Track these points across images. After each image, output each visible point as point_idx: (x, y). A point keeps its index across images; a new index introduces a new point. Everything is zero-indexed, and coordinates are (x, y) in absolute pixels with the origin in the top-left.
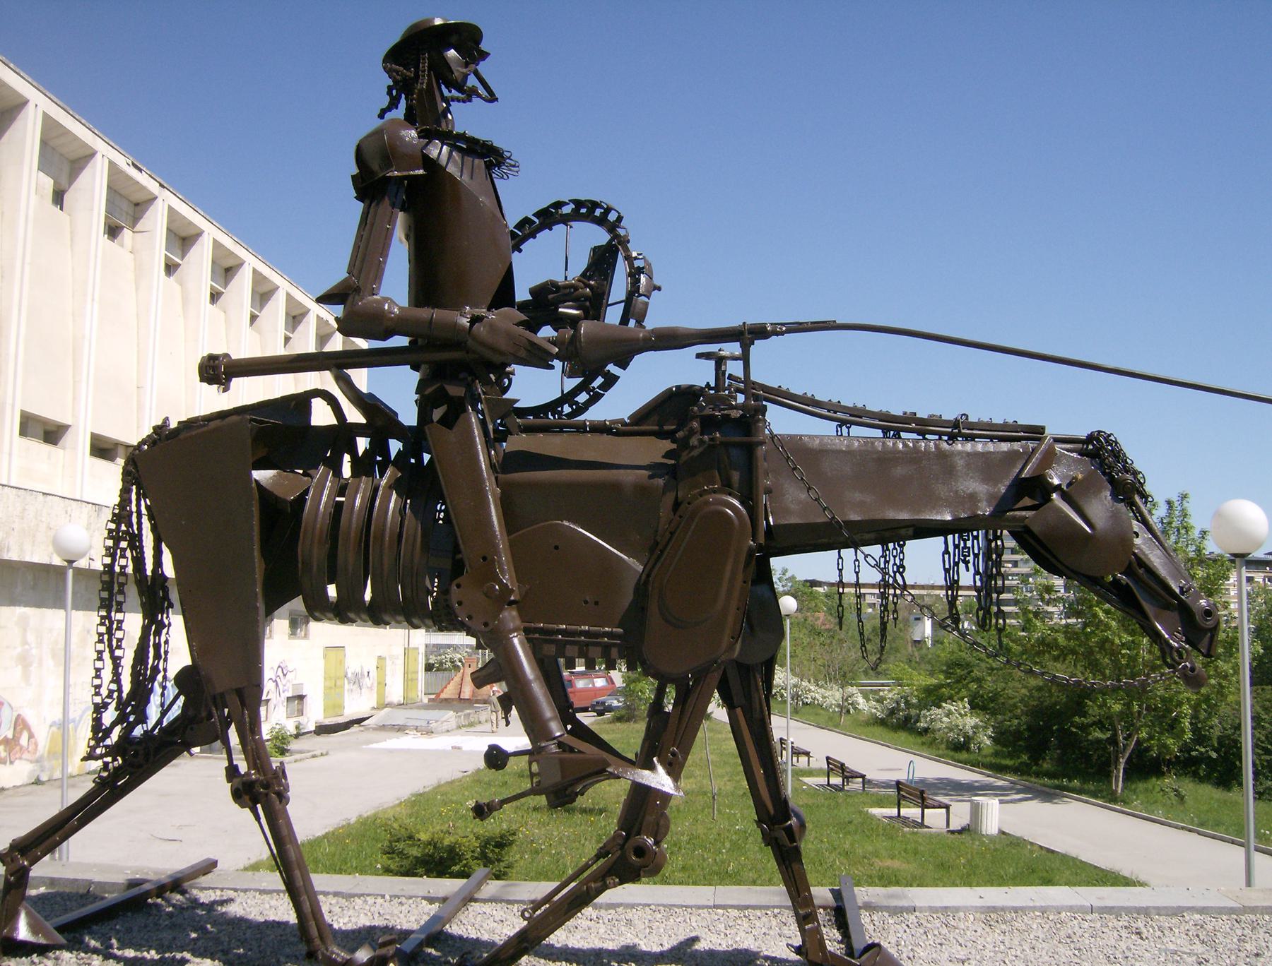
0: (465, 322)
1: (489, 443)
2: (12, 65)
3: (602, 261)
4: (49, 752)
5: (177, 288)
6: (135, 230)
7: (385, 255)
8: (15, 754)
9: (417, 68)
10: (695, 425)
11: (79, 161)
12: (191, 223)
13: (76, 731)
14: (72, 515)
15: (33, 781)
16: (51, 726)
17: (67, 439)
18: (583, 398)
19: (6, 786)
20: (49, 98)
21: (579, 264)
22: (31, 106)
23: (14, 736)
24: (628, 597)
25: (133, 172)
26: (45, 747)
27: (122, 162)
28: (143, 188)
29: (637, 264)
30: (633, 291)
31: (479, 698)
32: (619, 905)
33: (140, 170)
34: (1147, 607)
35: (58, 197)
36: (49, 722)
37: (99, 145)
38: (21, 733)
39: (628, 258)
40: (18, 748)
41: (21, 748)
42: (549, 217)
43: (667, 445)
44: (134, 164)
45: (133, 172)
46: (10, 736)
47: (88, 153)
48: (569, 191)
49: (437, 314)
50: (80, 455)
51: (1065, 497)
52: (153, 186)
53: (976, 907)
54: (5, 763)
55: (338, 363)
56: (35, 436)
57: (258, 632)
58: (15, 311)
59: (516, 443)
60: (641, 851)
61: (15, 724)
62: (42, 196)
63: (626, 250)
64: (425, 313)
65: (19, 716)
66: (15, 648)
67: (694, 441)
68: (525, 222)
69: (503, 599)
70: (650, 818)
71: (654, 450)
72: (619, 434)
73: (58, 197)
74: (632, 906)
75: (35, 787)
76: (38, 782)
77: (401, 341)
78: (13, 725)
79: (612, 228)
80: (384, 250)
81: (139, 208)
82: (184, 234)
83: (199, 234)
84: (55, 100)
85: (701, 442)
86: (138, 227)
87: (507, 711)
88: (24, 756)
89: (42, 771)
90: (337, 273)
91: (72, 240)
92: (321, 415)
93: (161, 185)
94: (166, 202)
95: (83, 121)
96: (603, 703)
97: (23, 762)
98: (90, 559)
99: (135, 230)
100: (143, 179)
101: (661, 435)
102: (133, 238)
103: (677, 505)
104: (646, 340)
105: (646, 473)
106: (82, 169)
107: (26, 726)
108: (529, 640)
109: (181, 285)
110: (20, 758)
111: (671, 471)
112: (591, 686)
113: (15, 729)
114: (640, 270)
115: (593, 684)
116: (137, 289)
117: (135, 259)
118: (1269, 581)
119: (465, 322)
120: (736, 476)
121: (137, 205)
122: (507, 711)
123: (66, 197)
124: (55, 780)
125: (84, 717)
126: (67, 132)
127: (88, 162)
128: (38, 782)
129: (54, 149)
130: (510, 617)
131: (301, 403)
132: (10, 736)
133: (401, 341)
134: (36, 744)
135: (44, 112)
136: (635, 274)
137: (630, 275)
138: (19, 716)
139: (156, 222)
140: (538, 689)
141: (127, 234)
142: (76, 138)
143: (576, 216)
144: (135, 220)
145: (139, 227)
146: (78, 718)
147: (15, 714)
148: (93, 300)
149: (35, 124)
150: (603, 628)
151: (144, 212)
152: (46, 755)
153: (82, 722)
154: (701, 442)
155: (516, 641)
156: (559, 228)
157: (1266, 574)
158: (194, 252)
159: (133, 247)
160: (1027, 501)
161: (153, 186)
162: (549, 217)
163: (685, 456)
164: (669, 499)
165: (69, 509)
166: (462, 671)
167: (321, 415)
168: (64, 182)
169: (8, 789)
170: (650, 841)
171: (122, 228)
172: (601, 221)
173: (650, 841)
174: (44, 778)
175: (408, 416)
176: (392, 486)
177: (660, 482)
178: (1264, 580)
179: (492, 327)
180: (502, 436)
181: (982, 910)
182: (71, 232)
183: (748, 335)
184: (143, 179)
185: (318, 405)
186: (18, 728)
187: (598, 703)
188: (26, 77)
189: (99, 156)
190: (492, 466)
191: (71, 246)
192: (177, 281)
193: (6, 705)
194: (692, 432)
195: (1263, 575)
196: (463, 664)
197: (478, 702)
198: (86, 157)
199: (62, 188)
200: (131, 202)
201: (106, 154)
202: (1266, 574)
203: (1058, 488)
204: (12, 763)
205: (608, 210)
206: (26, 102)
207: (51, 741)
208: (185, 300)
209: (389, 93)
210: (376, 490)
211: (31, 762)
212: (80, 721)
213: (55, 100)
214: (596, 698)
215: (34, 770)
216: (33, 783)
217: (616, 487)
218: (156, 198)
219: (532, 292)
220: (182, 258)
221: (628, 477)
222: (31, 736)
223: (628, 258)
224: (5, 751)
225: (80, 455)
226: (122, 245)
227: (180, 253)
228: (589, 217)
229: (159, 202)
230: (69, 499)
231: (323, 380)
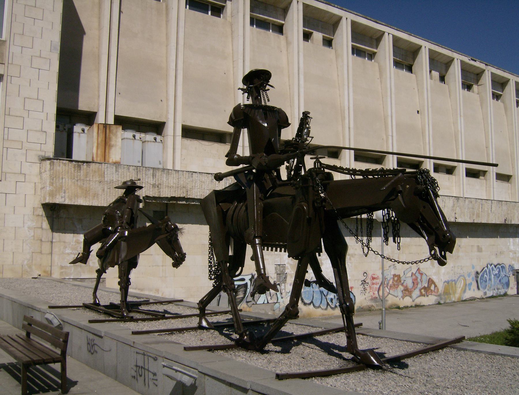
2: (413, 35)
4: (444, 292)
5: (502, 104)
6: (478, 85)
8: (429, 293)
11: (449, 62)
12: (503, 77)
13: (456, 284)
14: (446, 202)
15: (437, 303)
16: (444, 282)
17: (456, 171)
19: (425, 304)
20: (430, 43)
22: (423, 48)
23: (428, 286)
25: (472, 63)
26: (442, 290)
27: (466, 59)
28: (478, 68)
33: (476, 61)
35: (442, 79)
36: (443, 281)
37: (455, 55)
38: (431, 285)
40: (430, 291)
41: (431, 290)
44: (471, 59)
45: (472, 63)
46: (426, 286)
47: (451, 59)
50: (461, 177)
52: (482, 66)
53: (488, 352)
54: (425, 296)
56: (442, 172)
58: (427, 126)
61: (428, 282)
62: (435, 80)
65: (430, 278)
66: (427, 253)
73: (442, 79)
75: (438, 305)
76: (439, 303)
78: (427, 282)
81: (478, 76)
82: (502, 82)
83: (508, 80)
84: (433, 43)
86: (479, 83)
88: (433, 294)
89: (441, 299)
91: (450, 95)
93: (486, 65)
94: (489, 71)
95: (446, 48)
97: (433, 296)
98: (455, 218)
99: (478, 85)
100: (477, 64)
102: (478, 88)
106: (450, 66)
107: (433, 282)
109: (503, 103)
110: (431, 294)
113: (428, 283)
116: (482, 108)
117: (480, 96)
121: (477, 74)
123: (445, 78)
124: (447, 303)
125: (459, 279)
126: (440, 54)
127: (451, 64)
128: (439, 303)
129: (437, 61)
132: (426, 286)
134: (438, 289)
135: (429, 49)
138: (430, 278)
139: (487, 80)
141: (475, 87)
142: (444, 55)
144: (477, 81)
145: (479, 83)
146: (456, 280)
147: (428, 278)
148: (460, 116)
149: (426, 54)
150: (423, 230)
151: (481, 77)
152: (442, 293)
153: (458, 281)
158: (507, 88)
159: (478, 92)
161: (482, 66)
165: (444, 200)
168: (443, 72)
169: (426, 306)
171: (473, 85)
174: (442, 302)
181: (490, 353)
182: (449, 91)
184: (477, 64)
186: (430, 283)
188: (419, 37)
189: (455, 60)
191: (450, 97)
192: (501, 102)
193: (424, 274)
198: (451, 61)
199: (443, 75)
200: (474, 74)
201: (458, 58)
204: (427, 296)
206: (421, 47)
207: (444, 288)
208: (506, 109)
211: (436, 296)
212: (457, 281)
213: (433, 43)
215: (437, 299)
216: (437, 304)
218: (484, 70)
220: (502, 92)
222: (435, 286)
224: (425, 291)
225: (461, 177)
226: (473, 92)
227: (501, 90)
229: (486, 72)
230: (443, 196)
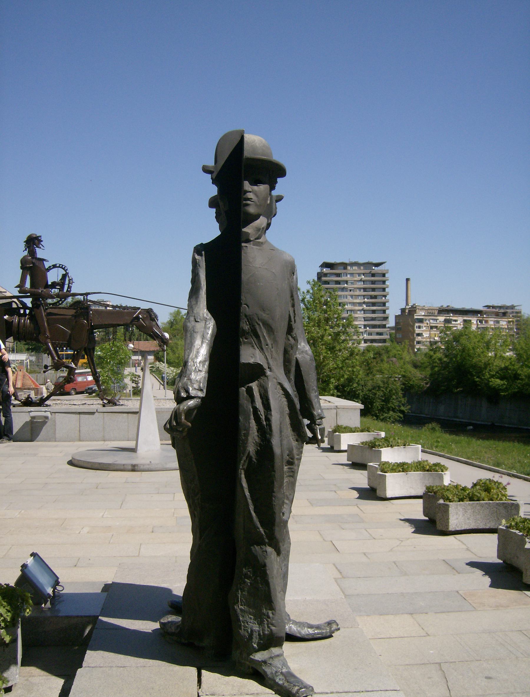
0: (40, 291)
1: (45, 312)
3: (64, 276)
7: (26, 280)
9: (30, 244)
10: (79, 309)
18: (60, 302)
21: (60, 277)
24: (68, 337)
29: (70, 278)
30: (69, 283)
31: (26, 387)
32: (71, 400)
34: (155, 337)
39: (69, 277)
42: (55, 266)
43: (75, 311)
48: (58, 262)
49: (36, 290)
51: (142, 320)
55: (17, 297)
57: (217, 327)
59: (49, 311)
60: (71, 378)
63: (68, 275)
64: (33, 290)
67: (79, 311)
68: (50, 267)
69: (47, 337)
70: (72, 373)
71: (72, 312)
72: (67, 309)
74: (74, 400)
77: (29, 294)
79: (66, 271)
80: (26, 279)
85: (80, 312)
87: (48, 355)
90: (18, 283)
92: (14, 306)
96: (92, 388)
101: (74, 309)
103: (76, 322)
104: (70, 295)
105: (71, 316)
108: (52, 344)
111: (75, 316)
112: (85, 380)
114: (70, 280)
115: (87, 379)
118: (479, 322)
119: (40, 291)
120: (86, 317)
122: (48, 355)
130: (49, 340)
131: (11, 303)
133: (29, 294)
136: (70, 280)
137: (69, 280)
140: (54, 352)
143: (59, 267)
154: (80, 312)
155: (50, 344)
156: (57, 269)
157: (478, 318)
160: (136, 320)
162: (55, 266)
163: (77, 314)
164: (75, 320)
166: (16, 373)
167: (14, 306)
170: (72, 377)
172: (64, 269)
173: (72, 377)
175: (30, 305)
176: (28, 319)
177: (73, 318)
178: (477, 321)
179: (45, 292)
180: (46, 309)
183: (87, 294)
185: (13, 303)
187: (89, 388)
190: (45, 316)
194: (78, 310)
195: (476, 319)
196: (16, 370)
197: (25, 389)
202: (478, 318)
203: (141, 318)
205: (65, 267)
209: (25, 247)
210: (25, 319)
214: (88, 386)
217: (65, 319)
219: (51, 283)
221: (68, 317)
223: (69, 277)
228: (62, 268)
231: (15, 300)
